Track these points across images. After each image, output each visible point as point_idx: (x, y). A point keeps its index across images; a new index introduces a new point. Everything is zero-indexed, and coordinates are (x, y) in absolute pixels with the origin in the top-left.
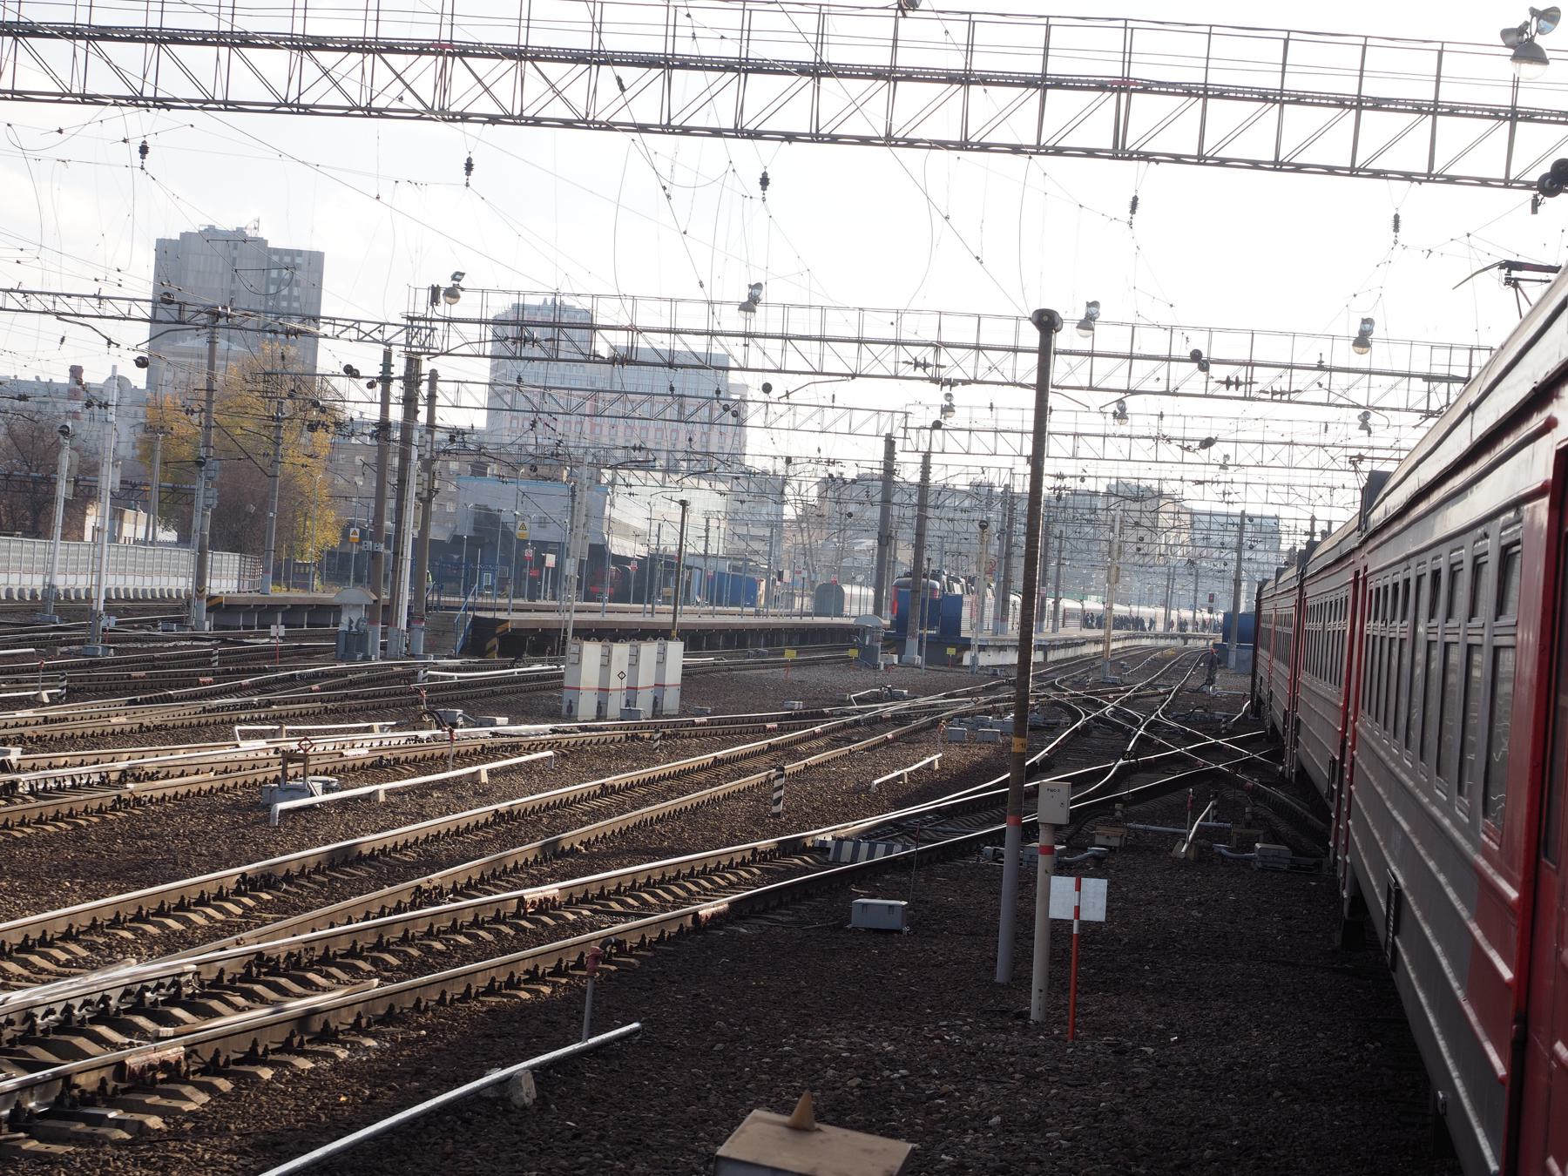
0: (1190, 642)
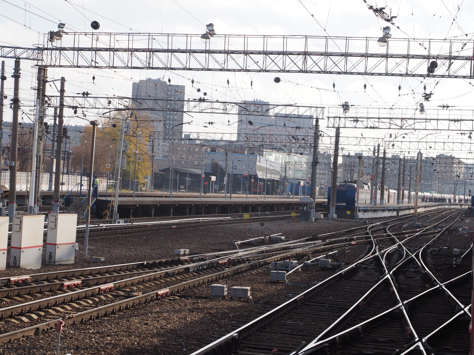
0: (463, 206)
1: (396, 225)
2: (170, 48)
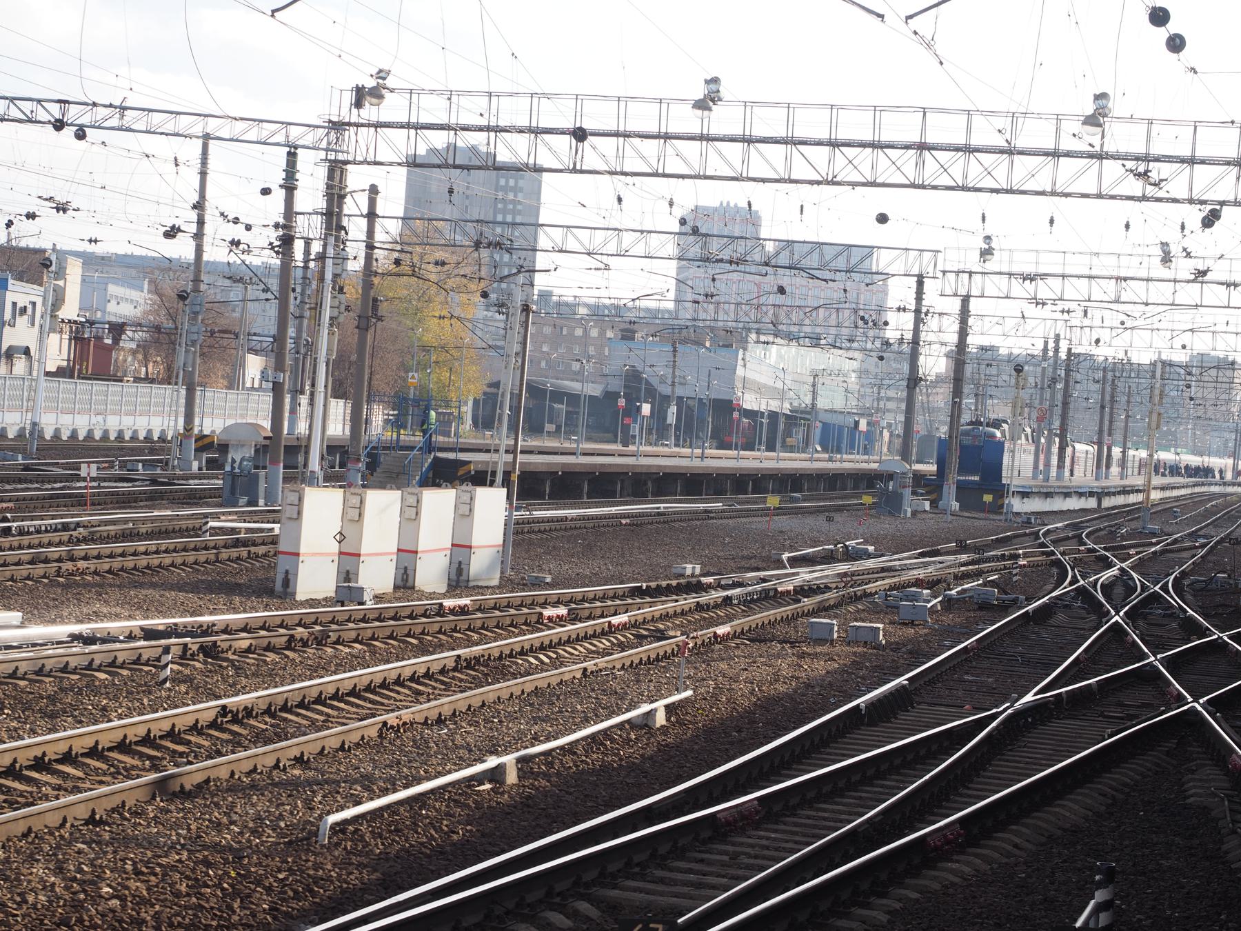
1: (1101, 529)
2: (621, 129)
